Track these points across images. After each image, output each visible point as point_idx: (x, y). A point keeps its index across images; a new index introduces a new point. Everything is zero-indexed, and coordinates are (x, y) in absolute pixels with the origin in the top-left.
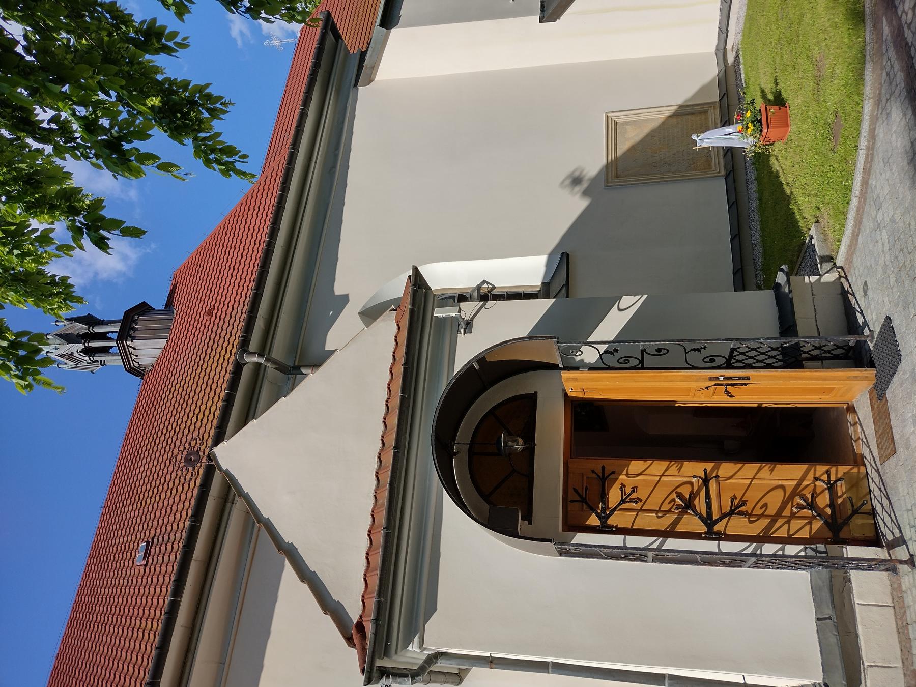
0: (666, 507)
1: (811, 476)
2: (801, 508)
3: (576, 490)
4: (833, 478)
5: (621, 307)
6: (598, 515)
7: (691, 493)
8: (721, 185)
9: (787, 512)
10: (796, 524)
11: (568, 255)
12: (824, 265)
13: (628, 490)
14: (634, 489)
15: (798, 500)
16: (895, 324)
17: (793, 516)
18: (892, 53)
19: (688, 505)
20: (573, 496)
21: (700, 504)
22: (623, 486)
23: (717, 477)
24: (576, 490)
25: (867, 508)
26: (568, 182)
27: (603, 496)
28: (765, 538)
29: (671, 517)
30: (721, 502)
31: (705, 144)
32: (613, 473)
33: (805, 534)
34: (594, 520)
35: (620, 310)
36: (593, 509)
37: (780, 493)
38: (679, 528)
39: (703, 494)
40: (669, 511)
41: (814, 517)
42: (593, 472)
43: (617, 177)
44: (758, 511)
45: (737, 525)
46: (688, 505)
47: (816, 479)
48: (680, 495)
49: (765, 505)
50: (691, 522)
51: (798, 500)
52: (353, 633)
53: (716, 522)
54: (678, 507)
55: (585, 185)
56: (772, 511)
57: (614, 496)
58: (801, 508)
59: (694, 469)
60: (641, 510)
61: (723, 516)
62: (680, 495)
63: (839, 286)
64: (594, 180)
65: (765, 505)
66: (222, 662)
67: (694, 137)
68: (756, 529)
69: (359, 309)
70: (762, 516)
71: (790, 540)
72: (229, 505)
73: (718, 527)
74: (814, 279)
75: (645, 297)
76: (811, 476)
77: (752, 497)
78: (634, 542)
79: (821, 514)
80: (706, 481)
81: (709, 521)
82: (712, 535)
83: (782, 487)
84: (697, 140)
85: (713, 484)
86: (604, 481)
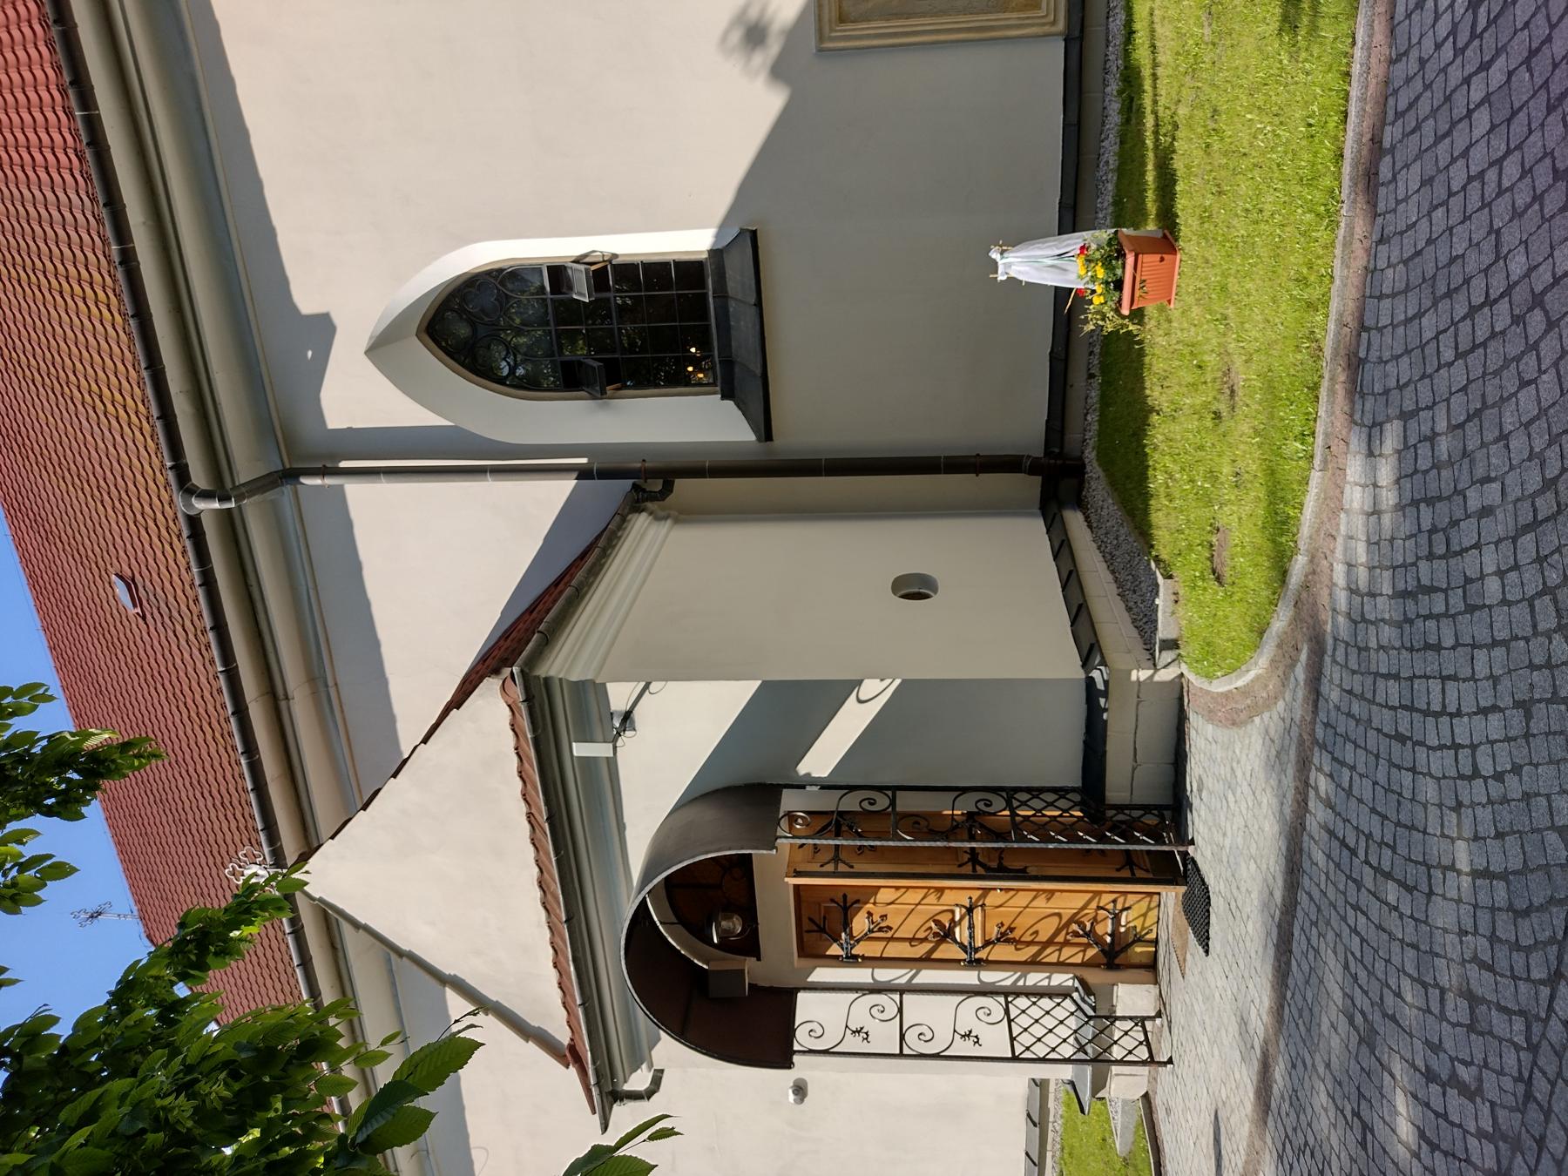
0: (921, 935)
1: (1094, 905)
2: (1076, 934)
3: (811, 919)
4: (1119, 906)
5: (862, 697)
6: (841, 946)
7: (952, 920)
8: (1055, 54)
9: (1060, 939)
10: (1067, 952)
11: (754, 234)
12: (1164, 653)
13: (876, 918)
14: (884, 917)
15: (1075, 927)
16: (1201, 950)
17: (1066, 943)
18: (1290, 771)
19: (946, 935)
20: (806, 925)
21: (961, 933)
22: (870, 914)
23: (983, 905)
24: (811, 919)
25: (1152, 936)
26: (736, 36)
27: (847, 924)
28: (1034, 963)
29: (927, 947)
30: (984, 926)
31: (1016, 272)
32: (857, 901)
33: (1078, 959)
34: (835, 950)
35: (860, 701)
36: (836, 939)
37: (1055, 920)
38: (934, 956)
39: (966, 922)
40: (925, 940)
41: (1088, 945)
42: (832, 901)
43: (842, 19)
44: (1027, 938)
45: (1002, 952)
46: (946, 935)
47: (1099, 908)
48: (937, 923)
49: (1037, 932)
50: (948, 951)
51: (1075, 927)
52: (570, 1056)
53: (977, 950)
54: (936, 934)
55: (774, 47)
56: (1043, 937)
57: (860, 924)
58: (1076, 934)
59: (958, 893)
60: (892, 939)
61: (987, 943)
62: (937, 923)
63: (1177, 689)
64: (793, 34)
65: (1037, 932)
66: (318, 680)
67: (995, 255)
68: (1026, 953)
69: (364, 343)
70: (1029, 944)
71: (1061, 966)
72: (283, 704)
73: (982, 955)
74: (1144, 674)
75: (898, 681)
76: (1094, 905)
77: (1022, 924)
78: (885, 975)
79: (1098, 941)
80: (970, 910)
81: (969, 949)
82: (975, 964)
83: (1059, 915)
84: (1000, 262)
85: (978, 913)
86: (847, 906)
